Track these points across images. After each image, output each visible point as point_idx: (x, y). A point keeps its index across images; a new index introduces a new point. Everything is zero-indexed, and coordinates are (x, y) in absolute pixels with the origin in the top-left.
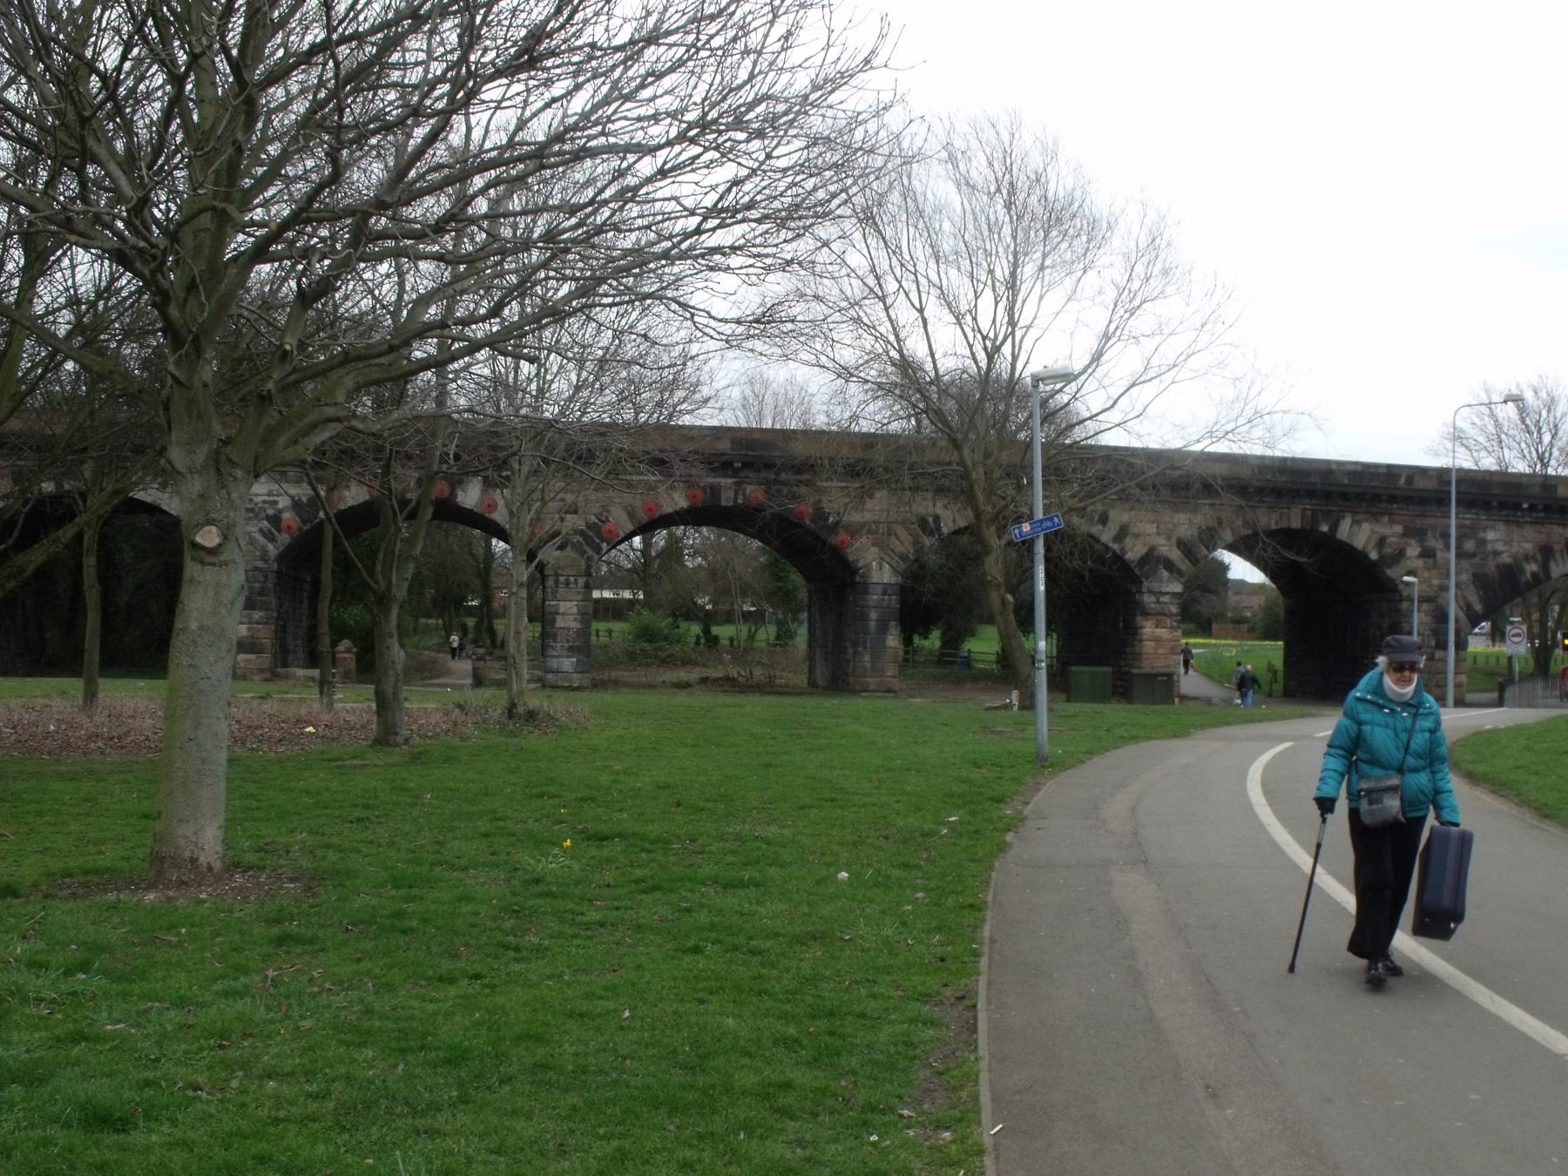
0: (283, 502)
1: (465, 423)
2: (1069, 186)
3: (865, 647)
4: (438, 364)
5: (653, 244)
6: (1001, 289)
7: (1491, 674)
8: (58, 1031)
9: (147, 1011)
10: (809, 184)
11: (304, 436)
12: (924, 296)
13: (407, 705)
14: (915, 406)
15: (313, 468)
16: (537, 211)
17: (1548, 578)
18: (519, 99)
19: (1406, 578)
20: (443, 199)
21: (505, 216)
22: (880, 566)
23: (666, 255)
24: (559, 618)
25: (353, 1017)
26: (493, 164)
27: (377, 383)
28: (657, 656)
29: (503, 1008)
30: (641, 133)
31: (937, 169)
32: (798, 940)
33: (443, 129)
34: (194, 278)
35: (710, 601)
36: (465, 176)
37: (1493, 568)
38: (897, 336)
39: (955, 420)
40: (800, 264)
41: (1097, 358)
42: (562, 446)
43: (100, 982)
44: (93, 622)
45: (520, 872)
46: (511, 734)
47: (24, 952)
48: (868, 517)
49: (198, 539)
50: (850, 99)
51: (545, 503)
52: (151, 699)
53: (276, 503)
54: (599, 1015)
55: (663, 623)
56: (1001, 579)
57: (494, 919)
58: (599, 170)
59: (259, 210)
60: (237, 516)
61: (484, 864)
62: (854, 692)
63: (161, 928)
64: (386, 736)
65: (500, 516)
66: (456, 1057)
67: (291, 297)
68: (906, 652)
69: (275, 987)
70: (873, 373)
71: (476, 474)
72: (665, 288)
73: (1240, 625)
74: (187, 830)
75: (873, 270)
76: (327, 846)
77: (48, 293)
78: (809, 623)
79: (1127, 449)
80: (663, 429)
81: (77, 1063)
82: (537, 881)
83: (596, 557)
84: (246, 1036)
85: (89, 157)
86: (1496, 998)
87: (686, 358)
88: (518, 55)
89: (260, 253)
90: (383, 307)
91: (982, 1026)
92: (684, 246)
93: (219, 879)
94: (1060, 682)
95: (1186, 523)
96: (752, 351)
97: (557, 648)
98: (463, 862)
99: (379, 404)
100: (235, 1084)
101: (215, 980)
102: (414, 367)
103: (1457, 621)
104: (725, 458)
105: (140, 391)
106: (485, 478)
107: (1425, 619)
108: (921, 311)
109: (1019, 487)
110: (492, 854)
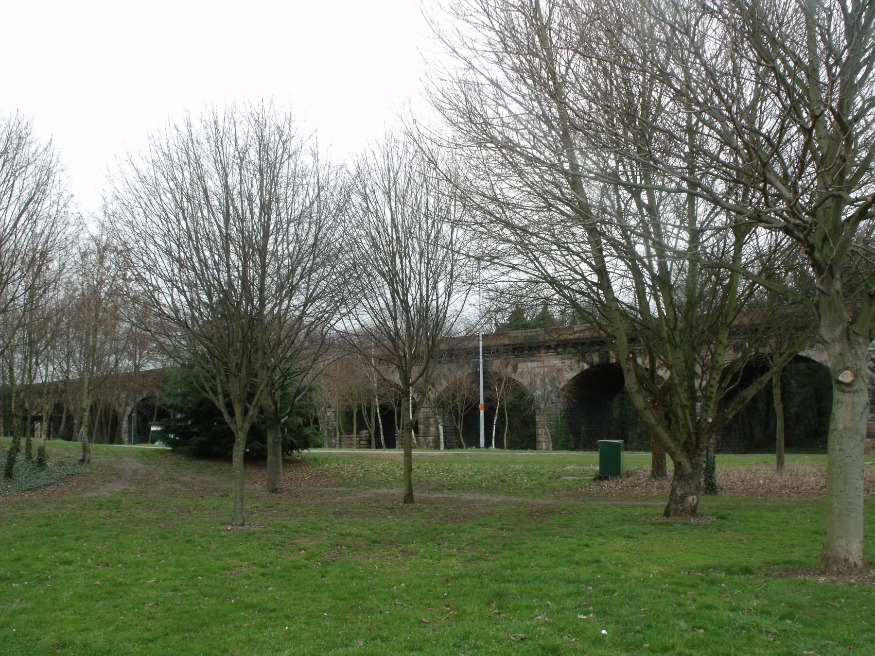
9: (826, 646)
34: (826, 235)
43: (798, 626)
47: (758, 605)
49: (840, 378)
52: (813, 466)
63: (830, 598)
74: (842, 542)
77: (747, 251)
93: (861, 572)
101: (864, 632)
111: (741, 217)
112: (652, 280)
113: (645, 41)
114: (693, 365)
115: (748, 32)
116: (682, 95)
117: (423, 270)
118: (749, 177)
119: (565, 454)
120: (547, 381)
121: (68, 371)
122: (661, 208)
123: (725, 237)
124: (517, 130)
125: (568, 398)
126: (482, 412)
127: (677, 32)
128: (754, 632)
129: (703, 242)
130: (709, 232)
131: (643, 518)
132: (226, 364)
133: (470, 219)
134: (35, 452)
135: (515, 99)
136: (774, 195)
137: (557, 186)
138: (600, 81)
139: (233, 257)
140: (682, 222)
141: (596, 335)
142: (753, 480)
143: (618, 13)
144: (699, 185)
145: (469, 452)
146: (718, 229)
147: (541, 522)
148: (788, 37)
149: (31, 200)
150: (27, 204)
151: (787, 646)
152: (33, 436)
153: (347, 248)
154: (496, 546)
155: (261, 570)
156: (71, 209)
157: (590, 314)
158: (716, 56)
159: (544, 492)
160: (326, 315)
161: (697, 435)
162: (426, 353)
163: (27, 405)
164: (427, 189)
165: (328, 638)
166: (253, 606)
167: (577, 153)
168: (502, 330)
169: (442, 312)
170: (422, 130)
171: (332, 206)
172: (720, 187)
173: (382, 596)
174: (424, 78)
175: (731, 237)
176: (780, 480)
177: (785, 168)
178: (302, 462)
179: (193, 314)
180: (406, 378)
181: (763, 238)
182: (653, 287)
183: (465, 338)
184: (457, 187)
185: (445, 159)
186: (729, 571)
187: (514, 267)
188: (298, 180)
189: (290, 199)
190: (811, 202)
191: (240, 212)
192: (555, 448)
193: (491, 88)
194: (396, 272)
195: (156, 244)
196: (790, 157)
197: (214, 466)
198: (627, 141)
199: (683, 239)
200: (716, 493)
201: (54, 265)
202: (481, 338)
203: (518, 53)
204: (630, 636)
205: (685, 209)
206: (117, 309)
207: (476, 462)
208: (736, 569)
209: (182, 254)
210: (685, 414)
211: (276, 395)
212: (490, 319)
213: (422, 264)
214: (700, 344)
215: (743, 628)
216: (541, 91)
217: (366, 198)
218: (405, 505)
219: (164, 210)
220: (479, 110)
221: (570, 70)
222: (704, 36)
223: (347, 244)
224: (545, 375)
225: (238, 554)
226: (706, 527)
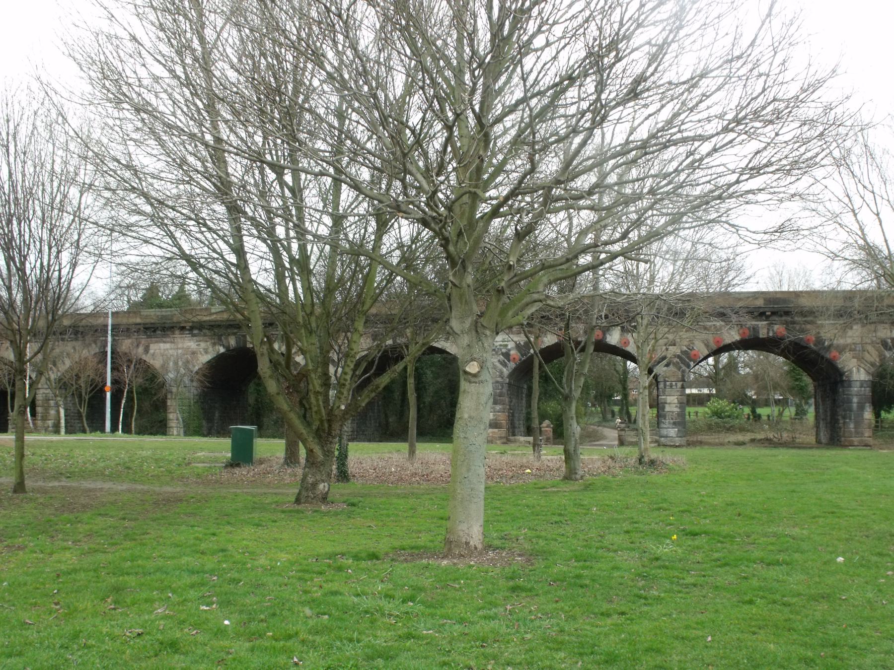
0: (511, 345)
3: (850, 419)
4: (593, 267)
8: (400, 632)
9: (443, 625)
10: (802, 150)
13: (582, 457)
15: (527, 327)
18: (631, 117)
21: (626, 182)
22: (858, 371)
23: (720, 197)
24: (667, 406)
27: (560, 279)
28: (724, 427)
32: (815, 598)
33: (589, 138)
34: (461, 230)
35: (755, 394)
42: (665, 309)
43: (420, 608)
44: (413, 413)
45: (647, 554)
46: (642, 474)
48: (849, 341)
49: (467, 369)
50: (825, 95)
51: (657, 341)
52: (443, 454)
53: (507, 345)
54: (693, 639)
57: (633, 580)
61: (627, 549)
62: (844, 446)
65: (631, 348)
68: (877, 422)
69: (511, 615)
74: (463, 527)
76: (539, 537)
77: (389, 241)
78: (816, 405)
81: (409, 650)
82: (657, 559)
83: (687, 370)
84: (496, 641)
85: (406, 171)
88: (628, 94)
89: (495, 213)
93: (481, 554)
97: (667, 423)
98: (615, 547)
99: (561, 291)
101: (479, 609)
102: (580, 269)
104: (761, 310)
106: (623, 328)
108: (878, 215)
110: (632, 543)
112: (290, 263)
117: (45, 237)
119: (197, 440)
120: (180, 363)
125: (201, 382)
126: (108, 395)
128: (378, 615)
135: (158, 61)
141: (232, 317)
145: (93, 437)
147: (167, 511)
151: (408, 628)
154: (116, 537)
159: (173, 478)
168: (135, 308)
172: (365, 174)
176: (411, 469)
180: (20, 354)
183: (90, 315)
186: (356, 557)
192: (186, 434)
202: (110, 315)
204: (253, 626)
207: (100, 447)
208: (363, 555)
210: (317, 400)
213: (44, 230)
215: (366, 612)
218: (15, 495)
226: (336, 514)
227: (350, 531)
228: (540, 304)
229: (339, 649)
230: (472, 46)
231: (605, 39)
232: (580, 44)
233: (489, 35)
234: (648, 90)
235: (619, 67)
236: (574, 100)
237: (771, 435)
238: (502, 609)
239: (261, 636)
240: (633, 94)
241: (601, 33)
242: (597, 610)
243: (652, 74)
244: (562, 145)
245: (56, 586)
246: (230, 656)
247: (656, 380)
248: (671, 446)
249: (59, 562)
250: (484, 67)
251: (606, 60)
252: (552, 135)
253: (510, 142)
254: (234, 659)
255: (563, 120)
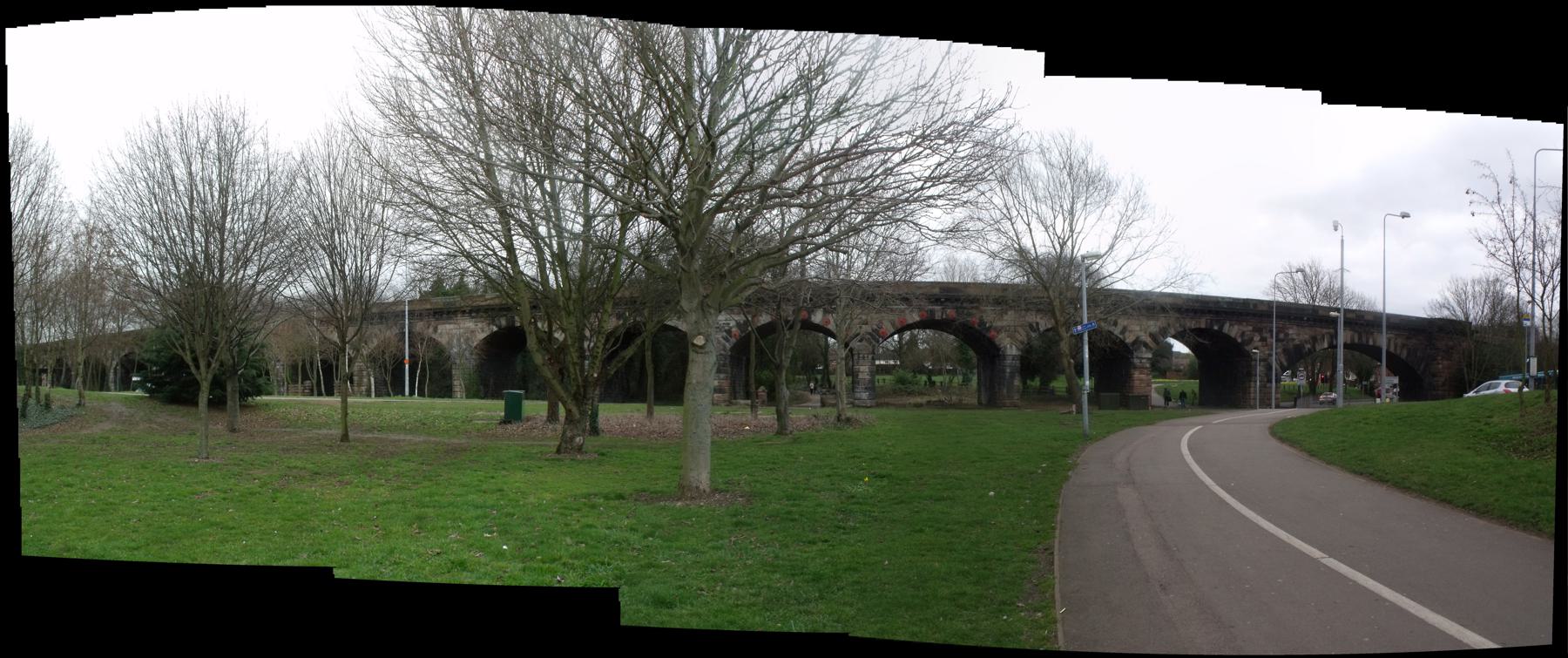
0: (732, 324)
1: (814, 283)
2: (1098, 165)
4: (801, 256)
5: (900, 195)
6: (1066, 215)
7: (1291, 394)
8: (643, 563)
9: (679, 555)
10: (975, 165)
11: (741, 292)
12: (1030, 218)
14: (1026, 271)
15: (744, 307)
16: (846, 181)
17: (1315, 350)
18: (834, 132)
19: (1254, 351)
20: (801, 178)
22: (1011, 347)
23: (907, 200)
25: (770, 559)
26: (825, 160)
27: (773, 266)
28: (906, 391)
29: (838, 555)
30: (894, 142)
31: (1036, 157)
36: (812, 166)
37: (1291, 346)
38: (1017, 237)
39: (1045, 277)
40: (971, 203)
41: (1112, 247)
42: (860, 293)
43: (658, 541)
44: (650, 381)
46: (839, 429)
48: (1005, 323)
49: (695, 342)
50: (994, 123)
53: (729, 324)
55: (909, 376)
56: (1067, 352)
57: (833, 514)
58: (875, 161)
59: (718, 189)
60: (712, 331)
64: (782, 430)
65: (831, 327)
66: (817, 578)
67: (733, 228)
68: (1024, 388)
70: (1006, 255)
71: (820, 307)
72: (907, 216)
73: (1178, 373)
75: (1006, 205)
76: (757, 481)
77: (630, 236)
79: (1125, 291)
80: (908, 284)
82: (853, 497)
83: (877, 345)
84: (723, 567)
86: (1290, 536)
87: (918, 249)
88: (832, 112)
89: (719, 208)
90: (775, 230)
91: (1056, 562)
92: (915, 196)
93: (708, 496)
94: (1095, 399)
95: (1153, 326)
96: (949, 245)
97: (860, 388)
98: (819, 489)
99: (774, 276)
100: (718, 588)
101: (708, 542)
103: (1276, 370)
105: (668, 275)
106: (824, 309)
107: (1262, 369)
108: (1029, 225)
109: (1076, 309)
110: (832, 484)
111: (626, 207)
113: (552, 49)
114: (583, 330)
115: (638, 48)
116: (581, 99)
117: (358, 244)
118: (634, 173)
119: (476, 402)
120: (462, 340)
121: (66, 332)
122: (561, 195)
123: (613, 223)
124: (440, 123)
126: (407, 366)
127: (579, 43)
128: (624, 545)
129: (595, 226)
130: (600, 218)
131: (539, 455)
132: (192, 325)
133: (399, 200)
134: (42, 397)
135: (439, 95)
136: (654, 190)
137: (474, 173)
138: (512, 82)
139: (197, 234)
140: (578, 208)
141: (504, 302)
142: (627, 424)
143: (529, 22)
144: (593, 178)
146: (608, 216)
147: (455, 458)
148: (670, 56)
149: (33, 193)
150: (31, 197)
152: (41, 385)
153: (293, 226)
154: (417, 478)
155: (223, 495)
156: (65, 199)
157: (499, 284)
158: (611, 67)
159: (458, 433)
160: (276, 283)
161: (585, 387)
162: (360, 315)
163: (35, 360)
164: (362, 173)
165: (278, 551)
166: (217, 524)
167: (491, 144)
169: (373, 282)
170: (358, 121)
171: (281, 189)
172: (610, 180)
173: (323, 518)
174: (359, 74)
175: (618, 224)
177: (663, 169)
178: (256, 407)
179: (164, 283)
181: (643, 225)
182: (552, 263)
183: (394, 303)
184: (388, 172)
185: (378, 147)
186: (607, 497)
187: (436, 243)
188: (251, 167)
189: (244, 183)
190: (682, 198)
191: (202, 195)
192: (467, 397)
193: (418, 85)
194: (335, 245)
195: (134, 226)
196: (667, 159)
197: (183, 409)
198: (534, 135)
199: (578, 223)
200: (598, 434)
201: (53, 246)
203: (442, 54)
204: (526, 551)
205: (580, 197)
206: (103, 281)
207: (402, 408)
209: (155, 233)
210: (575, 370)
211: (234, 351)
212: (414, 287)
214: (590, 313)
215: (616, 542)
216: (461, 88)
217: (309, 181)
219: (140, 196)
220: (407, 104)
221: (487, 71)
222: (601, 48)
223: (293, 222)
224: (461, 336)
225: (204, 482)
226: (589, 462)
227: (600, 476)
228: (757, 287)
229: (593, 570)
230: (701, 67)
231: (813, 64)
232: (793, 68)
233: (715, 58)
234: (849, 109)
235: (825, 88)
236: (787, 116)
237: (943, 398)
238: (727, 541)
239: (532, 559)
240: (837, 112)
241: (810, 58)
242: (804, 539)
243: (853, 96)
244: (776, 154)
245: (375, 513)
246: (507, 575)
247: (852, 352)
248: (863, 407)
249: (376, 495)
250: (711, 85)
251: (814, 82)
252: (768, 146)
253: (733, 151)
254: (510, 577)
255: (777, 133)
